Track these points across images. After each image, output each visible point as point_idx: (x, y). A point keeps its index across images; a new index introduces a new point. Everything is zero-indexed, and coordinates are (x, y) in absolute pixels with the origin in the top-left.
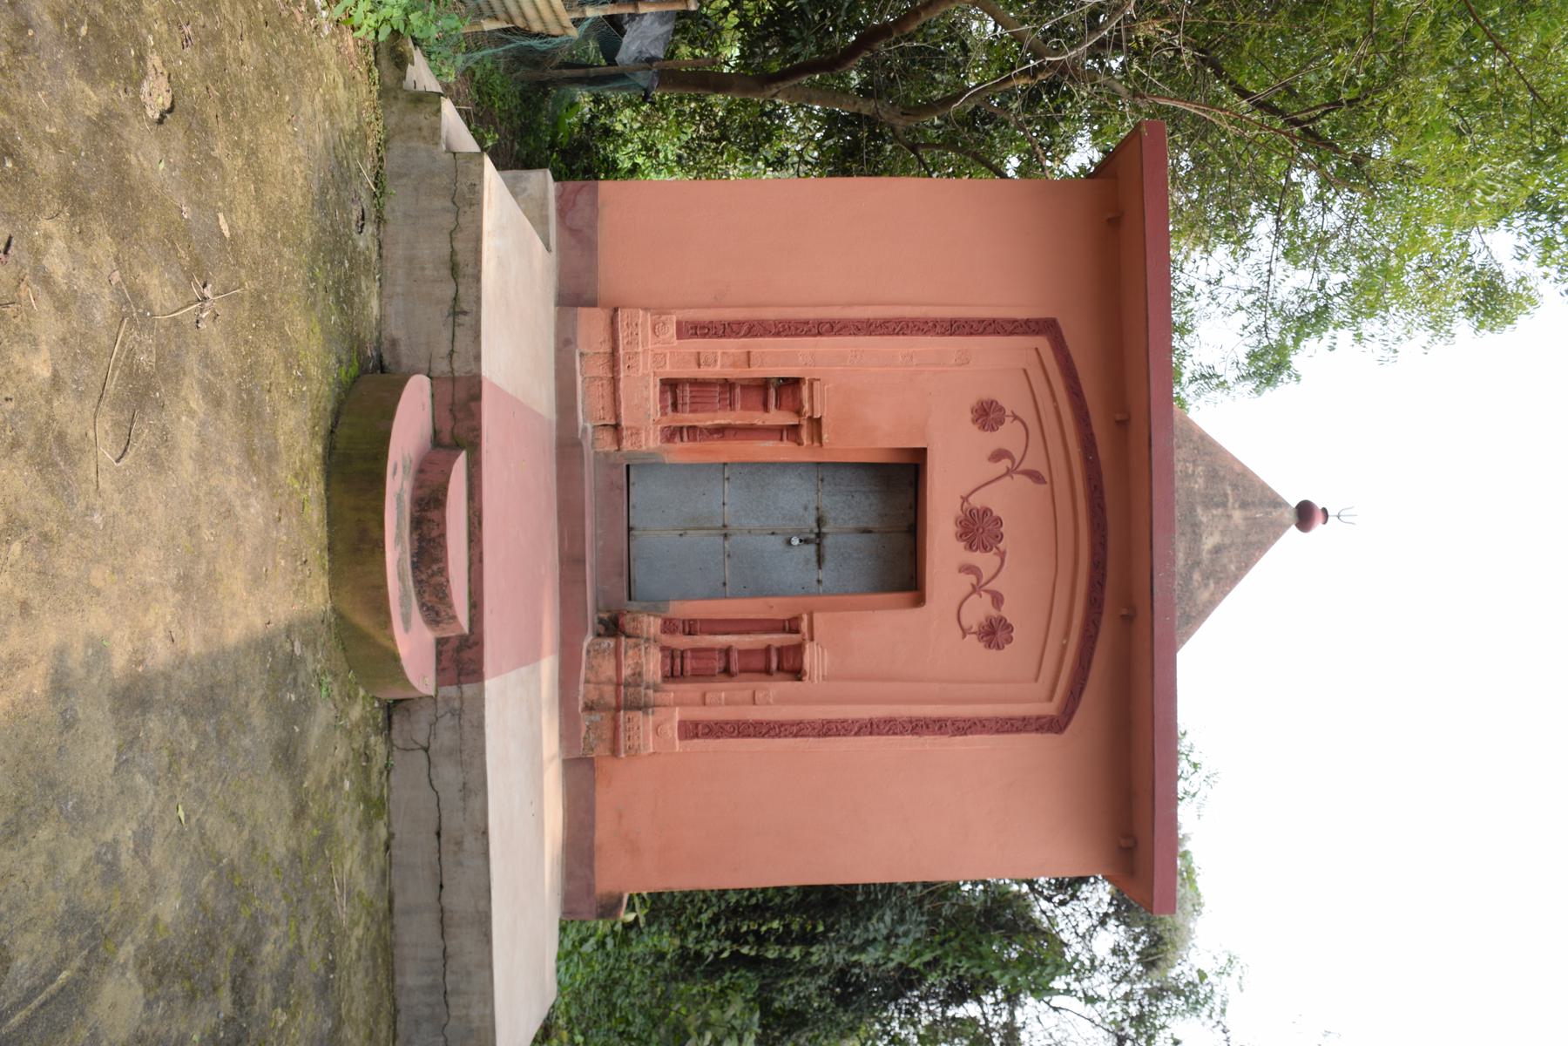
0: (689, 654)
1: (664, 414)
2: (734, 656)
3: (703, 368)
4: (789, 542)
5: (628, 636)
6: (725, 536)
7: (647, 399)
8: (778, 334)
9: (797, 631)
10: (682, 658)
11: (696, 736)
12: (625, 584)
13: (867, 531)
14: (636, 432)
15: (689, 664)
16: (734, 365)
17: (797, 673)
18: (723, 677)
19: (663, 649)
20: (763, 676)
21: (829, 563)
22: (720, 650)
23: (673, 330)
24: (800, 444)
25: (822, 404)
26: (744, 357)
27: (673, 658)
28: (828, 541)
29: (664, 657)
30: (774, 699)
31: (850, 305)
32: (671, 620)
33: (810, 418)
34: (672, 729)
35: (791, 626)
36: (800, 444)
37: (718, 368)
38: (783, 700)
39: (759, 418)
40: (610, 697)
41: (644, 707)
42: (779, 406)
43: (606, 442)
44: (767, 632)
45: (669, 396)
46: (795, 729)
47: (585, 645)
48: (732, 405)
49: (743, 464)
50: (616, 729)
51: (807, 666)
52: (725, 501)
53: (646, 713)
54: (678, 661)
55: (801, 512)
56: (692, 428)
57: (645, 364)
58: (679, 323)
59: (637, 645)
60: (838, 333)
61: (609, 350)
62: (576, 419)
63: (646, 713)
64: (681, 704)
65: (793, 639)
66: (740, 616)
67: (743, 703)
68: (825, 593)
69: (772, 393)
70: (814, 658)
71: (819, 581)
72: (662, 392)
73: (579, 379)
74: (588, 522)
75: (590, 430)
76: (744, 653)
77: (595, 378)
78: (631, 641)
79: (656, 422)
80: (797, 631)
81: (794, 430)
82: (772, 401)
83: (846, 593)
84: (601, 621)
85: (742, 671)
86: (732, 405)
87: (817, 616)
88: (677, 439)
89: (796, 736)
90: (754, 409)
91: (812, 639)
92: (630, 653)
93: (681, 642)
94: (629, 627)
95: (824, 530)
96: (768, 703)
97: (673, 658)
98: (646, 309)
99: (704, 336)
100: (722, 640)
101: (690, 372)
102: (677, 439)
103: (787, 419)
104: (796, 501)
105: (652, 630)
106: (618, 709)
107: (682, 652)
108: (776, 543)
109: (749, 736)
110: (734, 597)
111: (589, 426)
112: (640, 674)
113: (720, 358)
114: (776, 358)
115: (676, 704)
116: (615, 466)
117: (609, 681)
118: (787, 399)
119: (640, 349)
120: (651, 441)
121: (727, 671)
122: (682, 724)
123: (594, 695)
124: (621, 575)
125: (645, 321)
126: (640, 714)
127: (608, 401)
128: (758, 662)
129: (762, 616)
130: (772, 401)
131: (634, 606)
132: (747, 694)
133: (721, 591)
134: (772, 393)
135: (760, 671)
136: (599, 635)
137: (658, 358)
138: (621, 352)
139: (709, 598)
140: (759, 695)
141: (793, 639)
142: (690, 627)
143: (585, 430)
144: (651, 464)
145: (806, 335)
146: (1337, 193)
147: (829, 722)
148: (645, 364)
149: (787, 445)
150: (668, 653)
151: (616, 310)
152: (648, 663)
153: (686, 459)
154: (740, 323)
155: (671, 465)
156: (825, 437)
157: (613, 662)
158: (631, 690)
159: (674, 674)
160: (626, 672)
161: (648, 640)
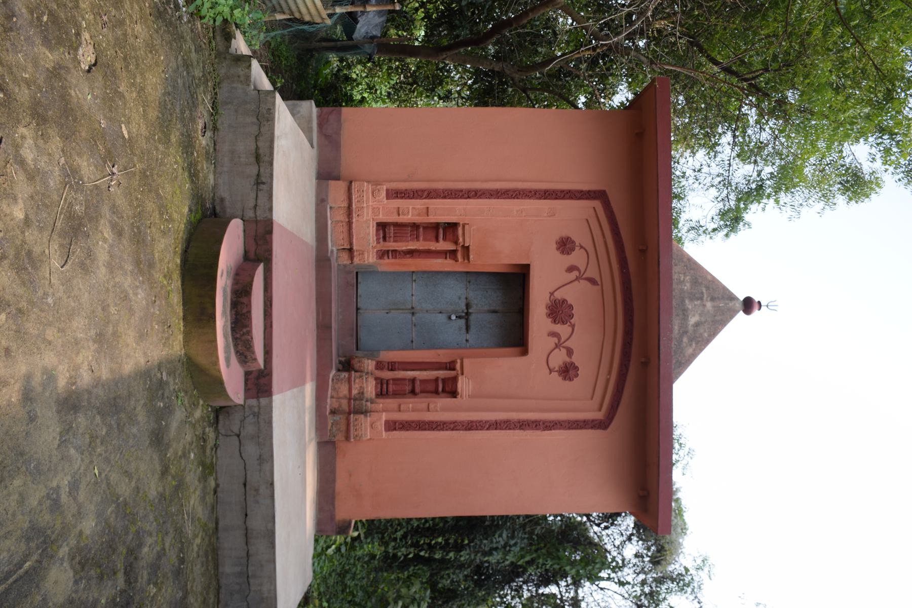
1: (378, 242)
2: (418, 383)
3: (401, 217)
4: (450, 318)
5: (356, 371)
6: (413, 314)
7: (369, 234)
8: (445, 197)
9: (454, 369)
11: (395, 429)
13: (495, 312)
14: (362, 253)
15: (391, 388)
16: (419, 215)
17: (454, 394)
18: (411, 395)
19: (376, 379)
20: (434, 395)
21: (473, 330)
22: (409, 380)
23: (384, 194)
25: (470, 238)
26: (425, 211)
27: (382, 384)
28: (472, 318)
30: (440, 408)
32: (381, 362)
33: (463, 246)
34: (381, 425)
35: (451, 366)
38: (444, 409)
39: (433, 246)
41: (365, 412)
42: (445, 239)
43: (344, 259)
44: (436, 369)
46: (452, 426)
47: (331, 376)
48: (417, 238)
49: (424, 272)
50: (348, 425)
51: (459, 390)
52: (413, 293)
53: (366, 416)
54: (385, 386)
56: (394, 251)
58: (387, 190)
60: (480, 197)
62: (327, 245)
63: (366, 416)
64: (387, 410)
66: (420, 360)
68: (470, 348)
69: (441, 231)
70: (464, 385)
71: (467, 341)
73: (329, 222)
74: (333, 305)
75: (335, 251)
76: (423, 382)
78: (358, 374)
79: (374, 248)
80: (454, 369)
82: (441, 236)
83: (482, 347)
84: (340, 362)
85: (422, 392)
86: (417, 238)
87: (466, 361)
88: (386, 257)
91: (462, 374)
92: (357, 381)
93: (387, 375)
94: (357, 366)
96: (437, 411)
97: (382, 384)
98: (368, 182)
99: (402, 198)
101: (394, 218)
102: (386, 257)
103: (449, 246)
104: (454, 294)
105: (370, 368)
106: (349, 413)
107: (387, 381)
108: (442, 318)
109: (425, 429)
110: (417, 349)
111: (335, 249)
112: (363, 393)
113: (412, 211)
114: (443, 211)
115: (384, 411)
116: (349, 272)
117: (345, 397)
120: (370, 258)
121: (413, 392)
122: (387, 422)
123: (336, 405)
124: (352, 336)
127: (346, 235)
128: (431, 387)
130: (441, 236)
131: (359, 353)
132: (424, 405)
134: (441, 231)
135: (432, 392)
137: (375, 210)
138: (354, 206)
139: (403, 349)
140: (432, 406)
142: (392, 366)
143: (332, 251)
144: (370, 272)
145: (461, 198)
147: (472, 422)
149: (449, 261)
151: (351, 182)
152: (367, 387)
154: (423, 191)
155: (382, 272)
156: (471, 257)
158: (357, 402)
159: (381, 394)
160: (355, 392)
161: (367, 373)
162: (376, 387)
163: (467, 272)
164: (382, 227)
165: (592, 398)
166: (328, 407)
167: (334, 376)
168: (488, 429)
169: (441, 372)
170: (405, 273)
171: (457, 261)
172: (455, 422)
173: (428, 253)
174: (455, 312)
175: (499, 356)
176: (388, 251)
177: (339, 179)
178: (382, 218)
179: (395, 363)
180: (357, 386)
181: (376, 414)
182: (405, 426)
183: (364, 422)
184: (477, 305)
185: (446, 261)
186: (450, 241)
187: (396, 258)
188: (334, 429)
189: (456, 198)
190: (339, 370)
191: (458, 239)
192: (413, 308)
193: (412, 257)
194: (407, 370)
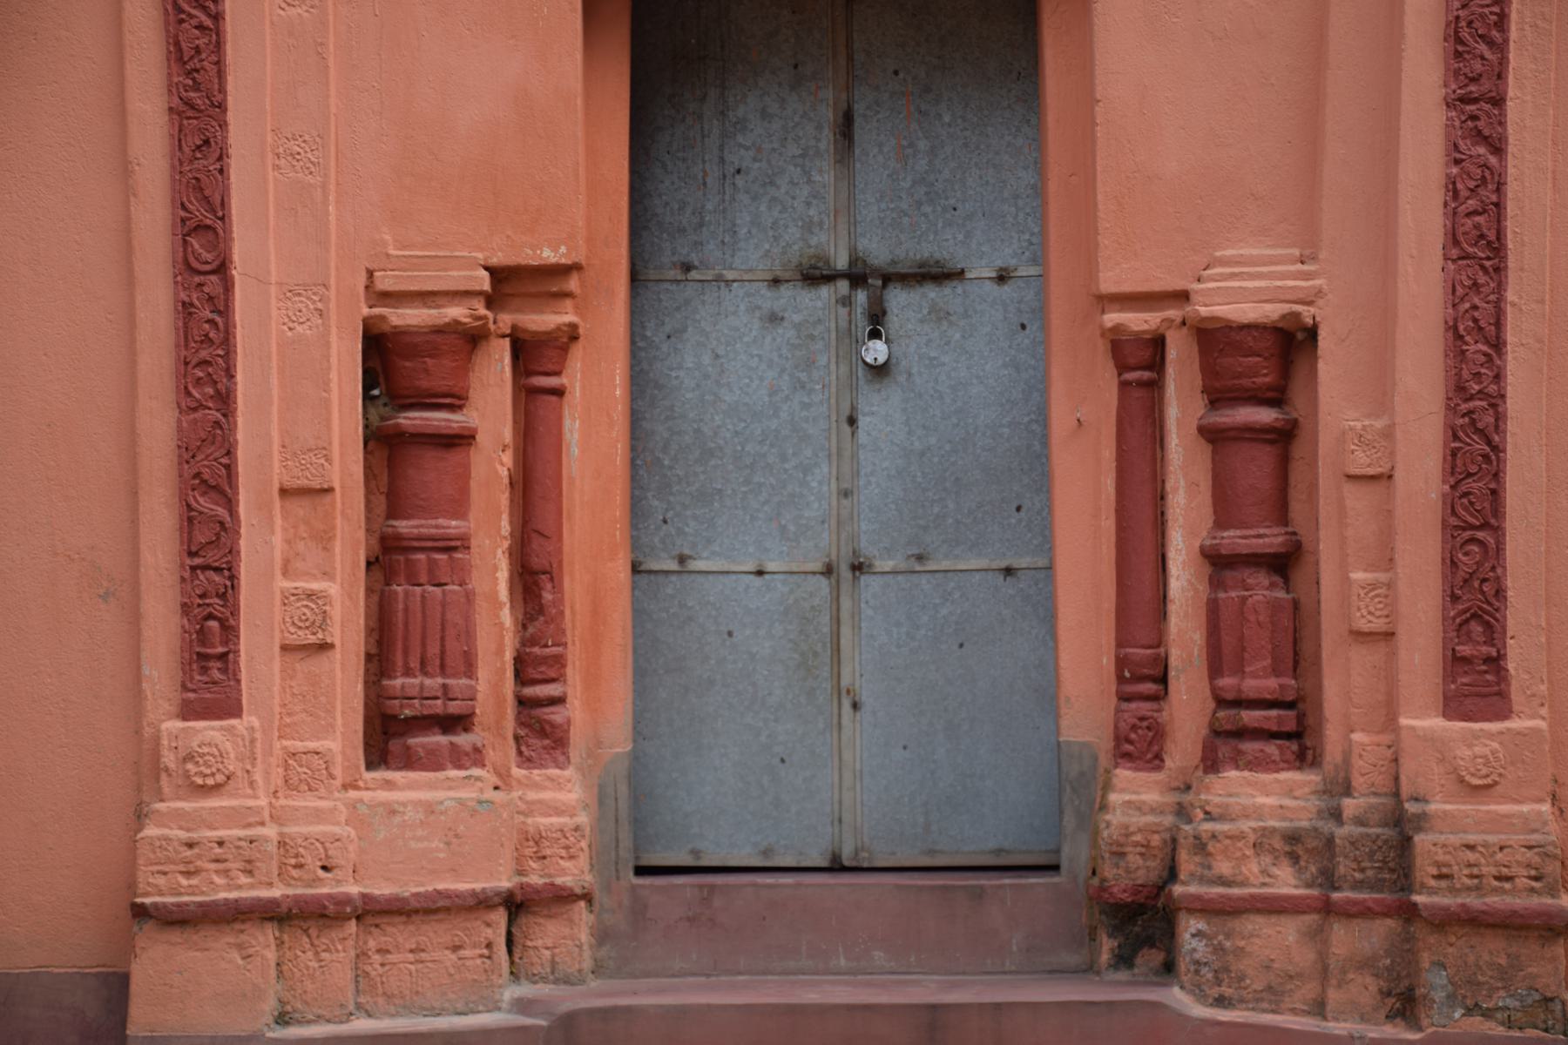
0: (1226, 682)
1: (476, 756)
2: (1234, 539)
3: (335, 635)
4: (880, 371)
5: (1172, 874)
6: (858, 568)
7: (430, 808)
8: (225, 400)
9: (1157, 343)
10: (1240, 703)
11: (1496, 662)
12: (1007, 880)
13: (846, 127)
14: (533, 844)
15: (1259, 683)
16: (324, 539)
17: (1292, 343)
18: (1300, 576)
19: (1211, 763)
20: (1298, 450)
21: (944, 247)
22: (1216, 583)
23: (208, 731)
24: (572, 334)
25: (446, 264)
26: (300, 508)
27: (1242, 733)
28: (878, 250)
29: (1236, 761)
30: (1376, 414)
31: (125, 170)
32: (1120, 739)
33: (491, 301)
34: (1474, 741)
35: (1140, 362)
36: (573, 334)
37: (333, 589)
38: (1379, 389)
39: (493, 460)
40: (1373, 936)
41: (1401, 828)
42: (455, 401)
43: (564, 938)
44: (1157, 438)
45: (422, 741)
46: (1475, 347)
47: (1200, 1011)
48: (453, 546)
49: (637, 510)
50: (1475, 921)
51: (1271, 312)
52: (749, 567)
53: (1421, 821)
54: (1250, 717)
55: (786, 333)
56: (523, 669)
57: (318, 816)
58: (189, 711)
59: (1200, 846)
60: (220, 209)
61: (270, 932)
62: (486, 1034)
63: (1421, 821)
64: (1387, 706)
65: (1180, 357)
66: (1109, 524)
67: (1387, 513)
68: (1039, 258)
69: (412, 419)
70: (1243, 292)
71: (1002, 278)
73: (362, 1025)
74: (811, 997)
75: (524, 990)
76: (1225, 510)
77: (360, 976)
78: (1187, 863)
79: (504, 782)
80: (1157, 343)
81: (525, 350)
82: (438, 419)
83: (1039, 191)
84: (1124, 960)
85: (1281, 514)
86: (453, 546)
87: (1109, 282)
88: (556, 715)
89: (1498, 345)
90: (464, 477)
91: (1183, 296)
92: (1224, 867)
93: (1188, 708)
94: (1143, 870)
95: (842, 263)
96: (1388, 434)
97: (1242, 733)
98: (140, 816)
99: (229, 631)
100: (1184, 578)
101: (343, 677)
102: (556, 715)
103: (494, 373)
104: (750, 352)
105: (1152, 797)
106: (1409, 912)
107: (1221, 702)
108: (882, 412)
109: (1496, 495)
110: (1046, 541)
111: (510, 992)
112: (1293, 838)
113: (303, 578)
114: (300, 409)
115: (1390, 722)
116: (639, 912)
117: (1317, 936)
118: (435, 374)
119: (270, 831)
120: (562, 797)
121: (1284, 563)
122: (1454, 706)
123: (1364, 989)
124: (979, 894)
125: (179, 815)
126: (1421, 840)
127: (434, 934)
128: (1255, 465)
129: (1108, 453)
130: (438, 419)
131: (1075, 854)
132: (1358, 500)
133: (1029, 581)
134: (412, 419)
135: (1284, 462)
136: (1169, 968)
137: (301, 773)
138: (276, 892)
139: (1050, 618)
140: (1361, 462)
141: (1180, 357)
142: (1143, 677)
143: (522, 1006)
144: (635, 798)
145: (225, 310)
146: (704, 162)
147: (1453, 238)
148: (318, 816)
149: (575, 375)
150: (1224, 750)
151: (140, 912)
152: (1258, 813)
153: (620, 687)
154: (190, 518)
155: (638, 734)
156: (549, 256)
157: (1254, 924)
158: (1344, 867)
159: (1297, 737)
160: (1286, 882)
161: (1182, 812)
162: (1259, 764)
163: (635, 278)
164: (388, 736)
165: (641, 871)
166: (1374, 1033)
167: (1201, 998)
168: (1498, 149)
169: (1172, 413)
170: (639, 614)
171: (572, 334)
172: (1453, 331)
173: (532, 487)
174: (850, 342)
175: (1087, 99)
176: (522, 702)
177: (124, 980)
178: (341, 736)
179: (1121, 663)
180: (1252, 868)
181: (1408, 768)
182: (1475, 604)
183: (1453, 828)
184: (809, 227)
185: (576, 393)
186: (464, 368)
187: (559, 661)
188: (1501, 999)
189: (227, 342)
190: (1169, 968)
191: (454, 327)
192: (828, 571)
193: (552, 574)
194: (1163, 599)
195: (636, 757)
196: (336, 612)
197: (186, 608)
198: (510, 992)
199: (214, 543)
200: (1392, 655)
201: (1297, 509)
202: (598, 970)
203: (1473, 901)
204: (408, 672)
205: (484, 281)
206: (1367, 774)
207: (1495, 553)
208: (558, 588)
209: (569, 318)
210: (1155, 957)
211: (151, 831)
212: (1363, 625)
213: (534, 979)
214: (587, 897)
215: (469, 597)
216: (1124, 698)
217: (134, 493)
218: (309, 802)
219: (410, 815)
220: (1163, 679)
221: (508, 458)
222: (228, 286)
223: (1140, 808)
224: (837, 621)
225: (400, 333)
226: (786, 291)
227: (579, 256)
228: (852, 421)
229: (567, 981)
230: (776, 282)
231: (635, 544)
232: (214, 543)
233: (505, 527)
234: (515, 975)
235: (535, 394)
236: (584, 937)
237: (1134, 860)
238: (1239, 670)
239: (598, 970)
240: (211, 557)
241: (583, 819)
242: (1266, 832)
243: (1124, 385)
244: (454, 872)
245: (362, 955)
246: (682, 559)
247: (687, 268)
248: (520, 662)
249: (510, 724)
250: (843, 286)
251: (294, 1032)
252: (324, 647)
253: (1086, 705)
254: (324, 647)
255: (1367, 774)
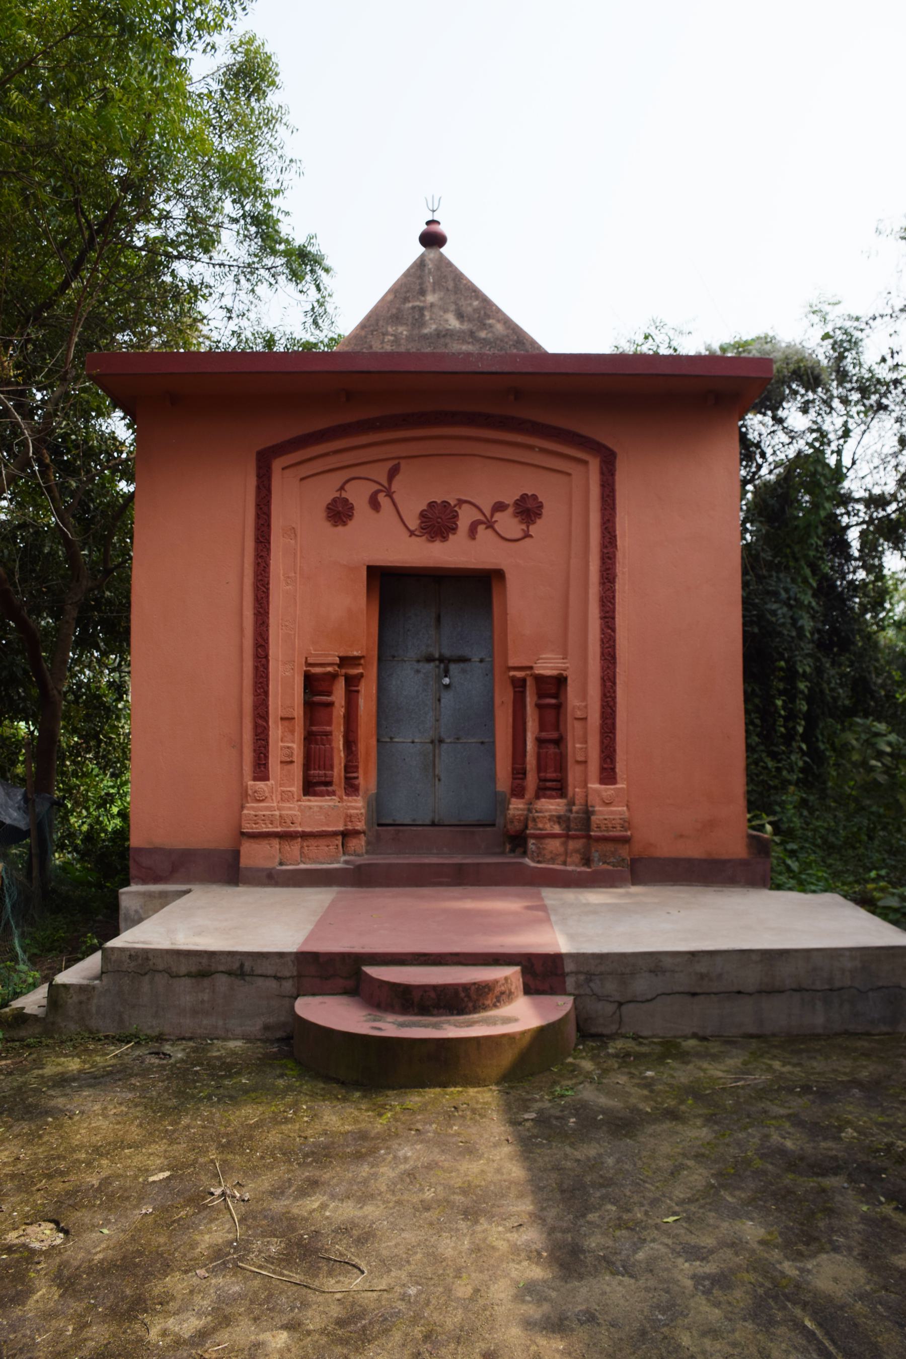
0: (542, 774)
1: (333, 793)
3: (295, 759)
4: (447, 687)
5: (526, 827)
7: (321, 807)
8: (266, 693)
11: (613, 769)
13: (438, 619)
14: (349, 818)
15: (551, 775)
16: (292, 732)
17: (560, 681)
19: (538, 797)
21: (466, 652)
22: (539, 747)
23: (260, 784)
26: (286, 723)
28: (447, 652)
29: (545, 797)
30: (582, 700)
32: (513, 790)
34: (608, 790)
35: (519, 686)
37: (295, 746)
38: (584, 696)
39: (339, 711)
41: (588, 813)
42: (329, 693)
43: (358, 844)
46: (609, 684)
47: (533, 864)
49: (379, 725)
51: (555, 672)
52: (410, 740)
53: (593, 813)
54: (548, 784)
55: (421, 675)
57: (290, 809)
60: (266, 640)
63: (593, 813)
66: (510, 730)
67: (585, 729)
68: (492, 655)
69: (318, 699)
70: (548, 666)
71: (481, 661)
72: (315, 794)
73: (302, 866)
74: (427, 861)
76: (542, 727)
77: (302, 853)
78: (531, 825)
80: (524, 680)
83: (492, 638)
84: (512, 851)
85: (557, 727)
86: (329, 734)
87: (512, 663)
88: (356, 782)
89: (614, 683)
90: (331, 714)
91: (531, 668)
92: (540, 826)
94: (518, 826)
95: (437, 656)
96: (586, 707)
98: (242, 807)
99: (266, 757)
101: (297, 770)
102: (356, 782)
103: (340, 688)
105: (521, 806)
106: (589, 837)
108: (447, 698)
111: (343, 858)
112: (559, 817)
113: (286, 743)
114: (286, 695)
115: (585, 786)
117: (565, 844)
119: (277, 813)
120: (357, 805)
122: (602, 781)
123: (576, 858)
125: (252, 808)
126: (593, 818)
127: (322, 842)
129: (510, 711)
131: (500, 821)
132: (577, 724)
133: (489, 747)
134: (318, 699)
137: (286, 797)
138: (279, 829)
139: (494, 756)
140: (579, 714)
142: (519, 773)
143: (346, 862)
148: (290, 809)
149: (362, 687)
151: (243, 834)
152: (550, 810)
154: (256, 726)
155: (379, 786)
156: (356, 654)
157: (548, 841)
158: (572, 825)
159: (559, 789)
160: (557, 829)
163: (380, 660)
164: (310, 787)
165: (379, 825)
166: (579, 869)
167: (533, 861)
168: (614, 630)
169: (528, 700)
170: (379, 753)
174: (439, 679)
176: (346, 778)
178: (296, 787)
179: (513, 769)
180: (548, 826)
183: (602, 814)
187: (357, 767)
188: (612, 860)
192: (432, 742)
195: (378, 794)
196: (295, 752)
197: (255, 751)
198: (343, 858)
199: (262, 733)
200: (586, 767)
201: (562, 727)
202: (367, 852)
203: (605, 834)
204: (319, 769)
205: (337, 660)
206: (579, 800)
207: (613, 740)
208: (356, 746)
209: (361, 671)
210: (521, 850)
211: (245, 812)
212: (579, 759)
213: (349, 855)
214: (364, 832)
215: (332, 749)
216: (514, 779)
217: (241, 718)
218: (287, 805)
219: (316, 809)
220: (525, 773)
221: (343, 710)
222: (268, 661)
223: (518, 809)
224: (434, 756)
225: (314, 675)
226: (421, 664)
227: (364, 654)
228: (439, 700)
229: (358, 855)
230: (418, 661)
231: (378, 734)
232: (262, 733)
233: (342, 729)
234: (344, 854)
235: (352, 682)
236: (363, 843)
237: (516, 823)
238: (545, 771)
239: (367, 852)
240: (262, 736)
241: (363, 811)
242: (552, 816)
243: (515, 692)
244: (328, 825)
245: (302, 847)
246: (391, 738)
247: (394, 657)
248: (346, 767)
249: (343, 785)
250: (437, 663)
251: (284, 867)
252: (292, 762)
253: (503, 781)
254: (292, 762)
255: (579, 800)
